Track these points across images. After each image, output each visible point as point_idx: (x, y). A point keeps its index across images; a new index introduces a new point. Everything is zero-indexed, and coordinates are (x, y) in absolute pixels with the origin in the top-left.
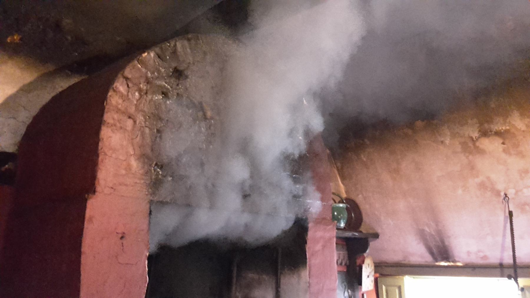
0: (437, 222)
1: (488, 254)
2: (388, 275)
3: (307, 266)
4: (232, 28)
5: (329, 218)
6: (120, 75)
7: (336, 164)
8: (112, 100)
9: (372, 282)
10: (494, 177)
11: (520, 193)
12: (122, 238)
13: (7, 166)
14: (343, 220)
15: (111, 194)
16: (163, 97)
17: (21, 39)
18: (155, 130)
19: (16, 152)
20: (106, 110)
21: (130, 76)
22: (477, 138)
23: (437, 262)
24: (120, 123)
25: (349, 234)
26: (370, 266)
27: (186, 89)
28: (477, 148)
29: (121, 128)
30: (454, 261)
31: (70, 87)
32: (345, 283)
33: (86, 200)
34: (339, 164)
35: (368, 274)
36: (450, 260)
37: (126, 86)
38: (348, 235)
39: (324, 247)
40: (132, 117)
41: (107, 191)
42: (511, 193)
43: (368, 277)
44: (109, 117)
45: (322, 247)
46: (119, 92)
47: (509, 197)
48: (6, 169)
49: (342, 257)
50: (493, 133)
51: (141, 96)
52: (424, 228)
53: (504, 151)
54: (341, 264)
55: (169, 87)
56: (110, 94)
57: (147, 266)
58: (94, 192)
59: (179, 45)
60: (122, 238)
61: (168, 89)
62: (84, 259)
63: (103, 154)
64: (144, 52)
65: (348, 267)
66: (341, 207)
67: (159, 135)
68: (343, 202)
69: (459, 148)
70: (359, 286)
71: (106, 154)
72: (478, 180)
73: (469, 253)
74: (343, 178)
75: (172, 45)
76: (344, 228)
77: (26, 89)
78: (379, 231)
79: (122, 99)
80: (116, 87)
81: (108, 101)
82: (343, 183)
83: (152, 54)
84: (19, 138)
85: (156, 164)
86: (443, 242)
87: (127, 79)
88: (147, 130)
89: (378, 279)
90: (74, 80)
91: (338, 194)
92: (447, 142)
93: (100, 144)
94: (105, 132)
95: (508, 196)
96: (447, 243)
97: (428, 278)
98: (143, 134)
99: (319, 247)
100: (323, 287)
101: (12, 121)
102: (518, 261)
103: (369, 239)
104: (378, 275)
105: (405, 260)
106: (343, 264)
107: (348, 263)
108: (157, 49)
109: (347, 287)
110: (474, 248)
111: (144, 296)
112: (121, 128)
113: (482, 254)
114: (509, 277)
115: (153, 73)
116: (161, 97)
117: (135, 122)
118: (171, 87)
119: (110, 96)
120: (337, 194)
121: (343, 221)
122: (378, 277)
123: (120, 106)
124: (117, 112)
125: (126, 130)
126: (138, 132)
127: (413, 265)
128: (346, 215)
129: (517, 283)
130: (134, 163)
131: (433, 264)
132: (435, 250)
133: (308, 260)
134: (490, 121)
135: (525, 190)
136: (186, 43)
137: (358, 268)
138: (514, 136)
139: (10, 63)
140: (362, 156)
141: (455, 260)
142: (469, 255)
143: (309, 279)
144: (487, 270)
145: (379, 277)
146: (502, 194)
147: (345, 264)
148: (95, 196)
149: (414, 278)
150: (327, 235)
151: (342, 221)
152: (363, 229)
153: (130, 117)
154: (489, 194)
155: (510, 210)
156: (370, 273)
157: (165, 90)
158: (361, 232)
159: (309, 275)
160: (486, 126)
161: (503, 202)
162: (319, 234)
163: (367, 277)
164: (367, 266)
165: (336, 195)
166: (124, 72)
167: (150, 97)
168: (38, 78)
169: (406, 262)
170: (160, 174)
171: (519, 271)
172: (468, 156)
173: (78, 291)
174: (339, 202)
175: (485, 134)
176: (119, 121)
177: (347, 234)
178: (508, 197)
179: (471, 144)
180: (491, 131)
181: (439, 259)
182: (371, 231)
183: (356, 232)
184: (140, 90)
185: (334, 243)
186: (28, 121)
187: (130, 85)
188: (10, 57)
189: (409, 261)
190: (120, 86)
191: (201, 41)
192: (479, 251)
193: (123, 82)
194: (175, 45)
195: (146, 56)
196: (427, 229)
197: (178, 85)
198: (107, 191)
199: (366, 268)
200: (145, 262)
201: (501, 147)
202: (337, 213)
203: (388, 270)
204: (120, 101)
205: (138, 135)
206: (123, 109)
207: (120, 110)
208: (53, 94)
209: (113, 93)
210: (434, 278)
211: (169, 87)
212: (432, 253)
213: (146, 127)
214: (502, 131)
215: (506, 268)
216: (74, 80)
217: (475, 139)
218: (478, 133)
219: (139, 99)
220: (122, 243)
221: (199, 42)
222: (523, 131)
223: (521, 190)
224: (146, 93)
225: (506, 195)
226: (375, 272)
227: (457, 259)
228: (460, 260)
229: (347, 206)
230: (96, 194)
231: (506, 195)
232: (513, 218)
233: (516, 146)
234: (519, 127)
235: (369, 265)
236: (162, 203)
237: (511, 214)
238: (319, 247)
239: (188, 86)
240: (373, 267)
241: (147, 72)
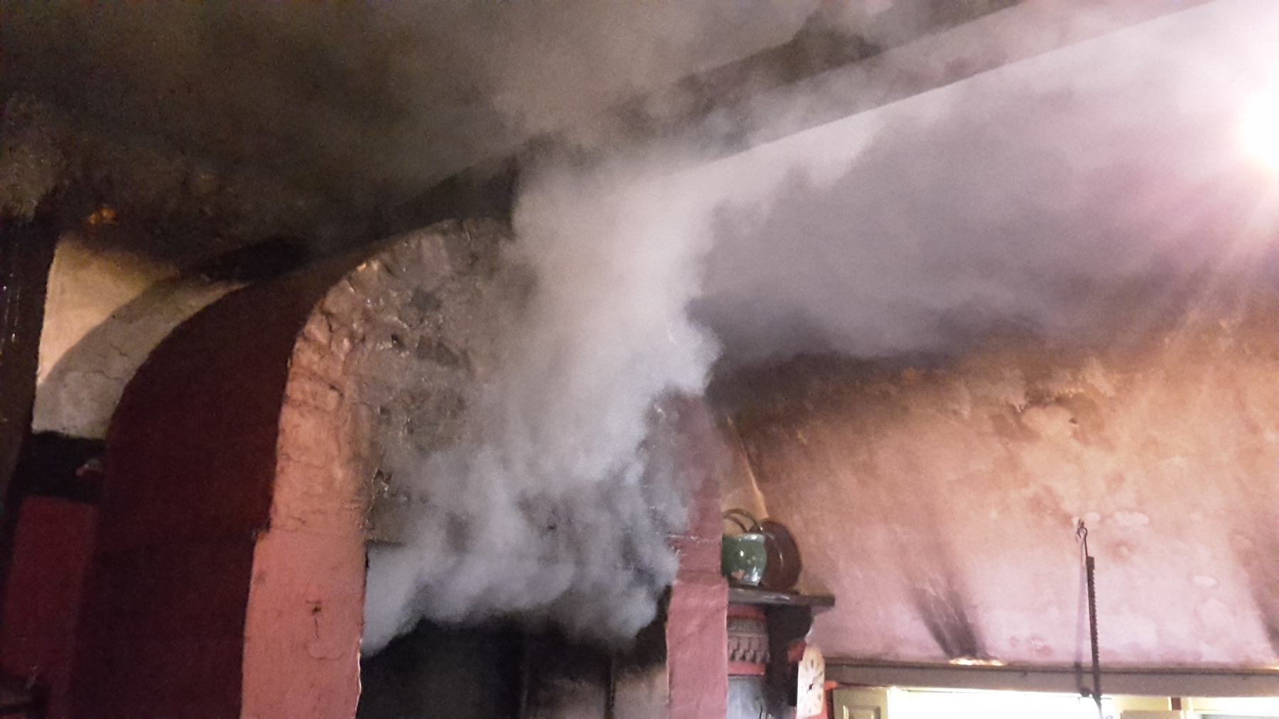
0: (950, 577)
1: (1052, 643)
2: (857, 685)
3: (667, 664)
4: (525, 144)
5: (714, 570)
6: (316, 310)
7: (747, 449)
8: (301, 356)
9: (819, 698)
10: (1059, 487)
11: (1109, 521)
12: (316, 610)
13: (86, 466)
14: (757, 568)
15: (297, 530)
16: (393, 344)
17: (116, 219)
18: (379, 410)
19: (104, 439)
20: (291, 376)
21: (334, 310)
22: (1022, 408)
23: (952, 659)
24: (314, 399)
25: (769, 598)
26: (815, 664)
28: (1023, 427)
29: (317, 408)
30: (986, 658)
31: (208, 309)
32: (762, 701)
33: (253, 544)
34: (752, 449)
35: (810, 682)
36: (978, 654)
37: (327, 329)
38: (771, 595)
39: (703, 627)
40: (337, 387)
41: (291, 524)
42: (1091, 519)
43: (810, 687)
44: (297, 388)
45: (698, 629)
46: (315, 341)
47: (1088, 530)
48: (88, 472)
49: (755, 645)
50: (1053, 399)
51: (354, 348)
52: (926, 588)
53: (1075, 435)
54: (753, 660)
55: (405, 326)
56: (297, 345)
57: (359, 664)
58: (267, 526)
59: (426, 244)
60: (316, 610)
61: (403, 329)
62: (247, 648)
63: (284, 457)
64: (360, 263)
65: (769, 669)
66: (753, 541)
67: (385, 417)
68: (758, 531)
69: (988, 427)
70: (791, 708)
71: (289, 458)
72: (1029, 492)
73: (1014, 641)
74: (762, 478)
75: (413, 246)
76: (760, 584)
77: (124, 315)
78: (835, 591)
79: (320, 354)
80: (309, 332)
81: (295, 357)
82: (761, 488)
83: (375, 266)
84: (108, 412)
85: (380, 473)
86: (962, 617)
87: (328, 314)
88: (364, 412)
89: (835, 693)
91: (748, 513)
92: (966, 412)
93: (280, 439)
94: (289, 417)
95: (1085, 526)
96: (969, 620)
97: (923, 691)
98: (356, 419)
99: (692, 627)
100: (698, 706)
101: (98, 379)
102: (1102, 659)
103: (813, 609)
104: (833, 684)
105: (886, 654)
106: (758, 660)
107: (768, 660)
108: (386, 256)
109: (764, 708)
110: (1024, 631)
111: (354, 717)
112: (317, 408)
113: (1040, 644)
114: (1085, 692)
115: (376, 301)
116: (391, 346)
117: (341, 395)
118: (410, 326)
119: (298, 350)
120: (745, 513)
121: (757, 571)
123: (315, 368)
124: (310, 379)
125: (324, 411)
126: (346, 414)
127: (907, 663)
128: (762, 558)
129: (1099, 704)
130: (339, 473)
131: (944, 662)
132: (948, 637)
133: (668, 654)
134: (1047, 376)
135: (1118, 516)
136: (440, 240)
137: (790, 669)
138: (1092, 406)
139: (95, 265)
140: (800, 436)
141: (987, 654)
142: (1014, 646)
143: (671, 689)
144: (1055, 676)
145: (837, 688)
146: (1075, 521)
147: (763, 661)
148: (269, 535)
149: (909, 691)
150: (712, 603)
151: (755, 569)
152: (802, 587)
153: (332, 388)
154: (1049, 521)
155: (1089, 555)
156: (815, 679)
157: (399, 333)
158: (797, 593)
159: (670, 682)
160: (1040, 386)
161: (1077, 539)
162: (693, 602)
163: (808, 687)
164: (809, 664)
165: (744, 515)
166: (323, 303)
167: (369, 345)
168: (145, 293)
169: (890, 658)
170: (385, 491)
171: (1103, 678)
172: (1007, 444)
173: (236, 710)
174: (752, 531)
175: (1037, 400)
176: (314, 395)
177: (767, 597)
178: (1086, 530)
179: (1011, 420)
180: (1049, 395)
181: (956, 651)
182: (819, 592)
183: (785, 591)
184: (352, 337)
185: (721, 620)
187: (334, 327)
188: (96, 253)
189: (897, 655)
190: (316, 328)
191: (467, 233)
192: (1034, 638)
193: (322, 320)
194: (419, 246)
195: (364, 271)
196: (930, 590)
197: (422, 321)
198: (291, 524)
199: (807, 669)
200: (356, 656)
201: (1068, 429)
203: (850, 675)
204: (316, 358)
205: (346, 420)
206: (320, 372)
207: (315, 374)
209: (303, 343)
210: (951, 692)
211: (405, 326)
212: (939, 636)
213: (362, 403)
214: (1071, 396)
215: (1106, 673)
217: (1019, 411)
218: (1026, 398)
219: (351, 351)
220: (316, 622)
221: (463, 235)
222: (1111, 398)
223: (1111, 516)
224: (363, 340)
225: (1082, 525)
226: (827, 678)
227: (991, 654)
228: (998, 656)
229: (767, 539)
230: (272, 530)
231: (1082, 525)
232: (1094, 571)
233: (1099, 427)
234: (1102, 390)
235: (812, 663)
236: (324, 467)
237: (1090, 563)
238: (692, 627)
239: (442, 321)
240: (822, 668)
241: (365, 300)
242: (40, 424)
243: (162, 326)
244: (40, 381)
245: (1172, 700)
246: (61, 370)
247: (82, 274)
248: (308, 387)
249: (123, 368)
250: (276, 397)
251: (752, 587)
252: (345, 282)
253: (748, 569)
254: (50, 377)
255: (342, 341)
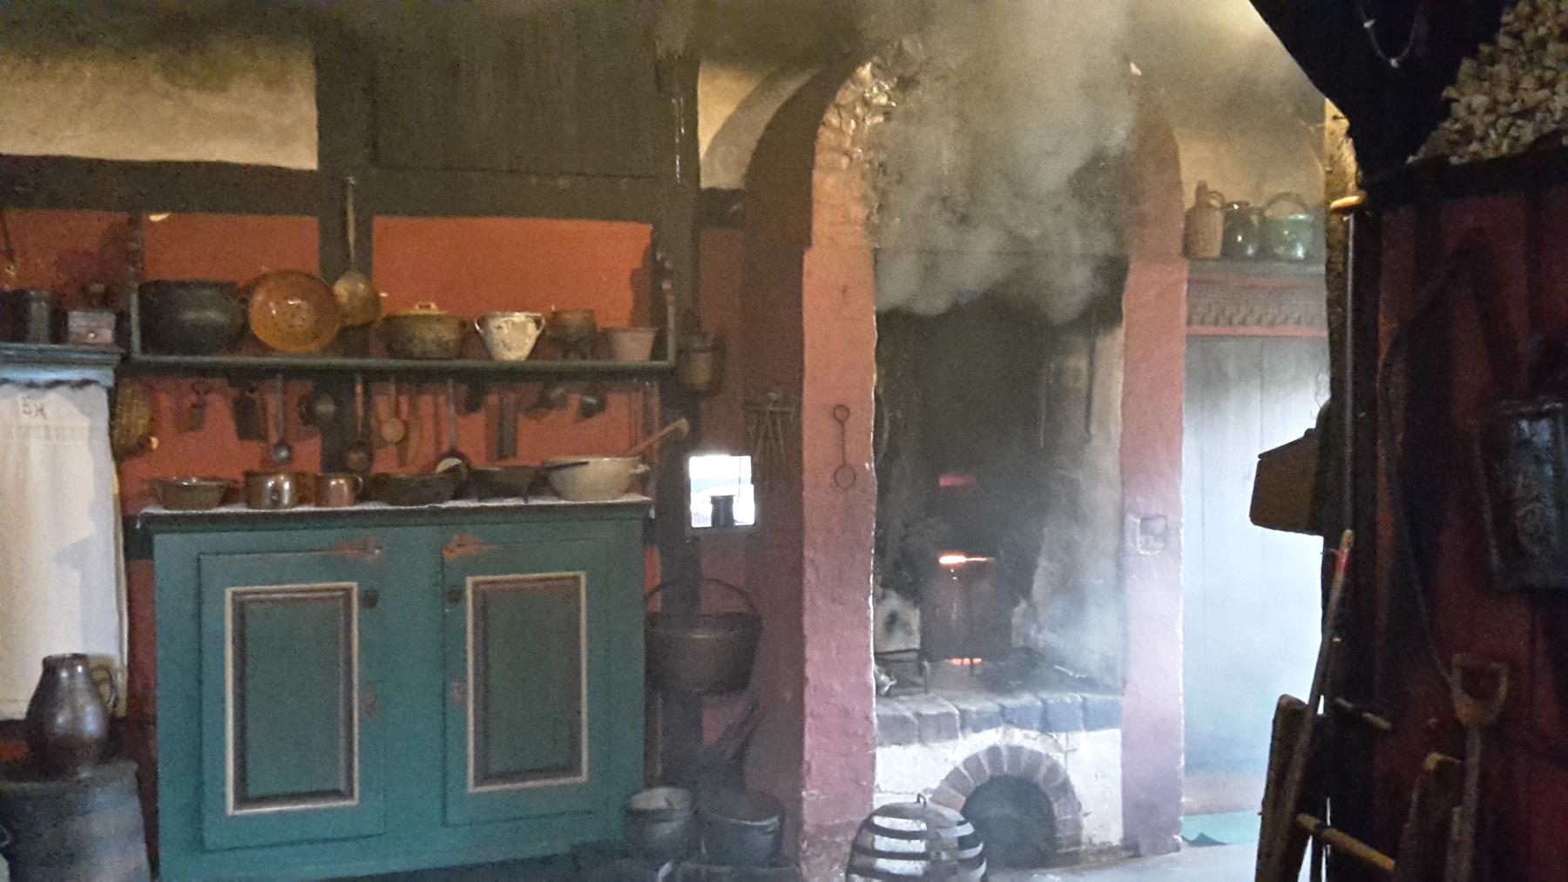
21: (842, 103)
27: (69, 867)
44: (821, 158)
58: (810, 244)
77: (746, 105)
84: (744, 170)
90: (803, 79)
93: (814, 192)
94: (817, 176)
108: (876, 59)
117: (851, 159)
122: (624, 330)
168: (756, 89)
184: (856, 117)
186: (753, 146)
202: (1236, 238)
208: (778, 105)
216: (803, 79)
242: (705, 184)
243: (766, 113)
244: (702, 155)
245: (457, 466)
246: (712, 148)
247: (717, 82)
248: (828, 156)
249: (750, 141)
250: (809, 166)
251: (1297, 261)
252: (849, 83)
253: (1291, 246)
254: (706, 155)
255: (850, 122)
